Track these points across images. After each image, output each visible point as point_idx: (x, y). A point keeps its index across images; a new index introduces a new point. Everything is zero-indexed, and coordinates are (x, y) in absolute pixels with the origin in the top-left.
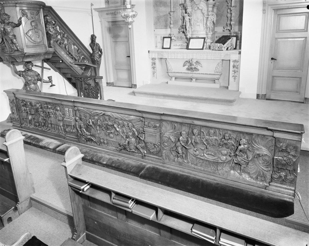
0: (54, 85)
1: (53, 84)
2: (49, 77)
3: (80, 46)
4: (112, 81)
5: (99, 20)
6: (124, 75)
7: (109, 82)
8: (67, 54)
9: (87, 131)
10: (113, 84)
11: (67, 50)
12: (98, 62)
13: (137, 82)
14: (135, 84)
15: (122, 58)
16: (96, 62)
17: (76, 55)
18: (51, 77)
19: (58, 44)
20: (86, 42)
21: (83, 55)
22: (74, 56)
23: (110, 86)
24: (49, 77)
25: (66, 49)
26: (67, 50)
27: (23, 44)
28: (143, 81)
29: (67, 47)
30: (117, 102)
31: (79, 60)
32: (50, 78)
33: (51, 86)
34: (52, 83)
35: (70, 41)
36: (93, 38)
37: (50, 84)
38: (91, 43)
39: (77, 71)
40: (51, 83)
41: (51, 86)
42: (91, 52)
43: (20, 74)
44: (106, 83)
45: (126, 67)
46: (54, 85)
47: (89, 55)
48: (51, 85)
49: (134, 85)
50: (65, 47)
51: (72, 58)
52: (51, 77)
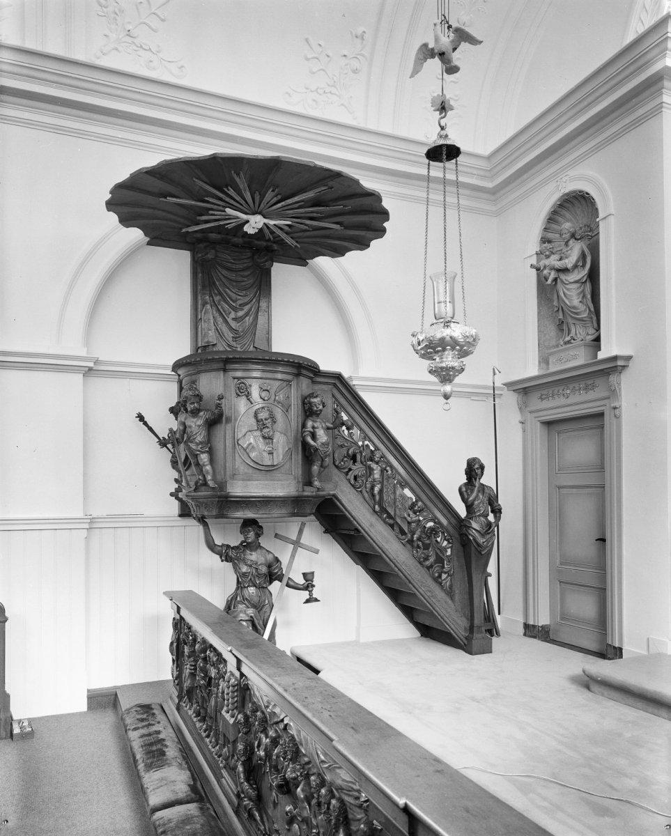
0: (316, 600)
1: (314, 596)
2: (304, 575)
3: (424, 491)
4: (543, 619)
5: (517, 417)
6: (584, 606)
7: (531, 622)
8: (374, 511)
9: (247, 780)
10: (548, 632)
11: (377, 498)
12: (479, 549)
13: (625, 639)
14: (617, 646)
15: (583, 548)
16: (473, 548)
17: (405, 518)
18: (313, 573)
19: (349, 481)
20: (449, 482)
21: (434, 519)
22: (399, 521)
23: (535, 637)
24: (304, 575)
25: (373, 495)
26: (377, 498)
27: (228, 470)
28: (648, 639)
29: (377, 489)
30: (333, 695)
31: (414, 534)
32: (308, 577)
33: (308, 601)
34: (311, 595)
35: (390, 472)
36: (473, 470)
37: (305, 595)
38: (465, 484)
39: (402, 569)
40: (308, 592)
41: (308, 601)
42: (463, 512)
43: (226, 554)
44: (522, 626)
45: (589, 577)
46: (316, 600)
47: (453, 520)
48: (308, 597)
49: (614, 648)
50: (372, 488)
51: (392, 526)
52: (313, 573)
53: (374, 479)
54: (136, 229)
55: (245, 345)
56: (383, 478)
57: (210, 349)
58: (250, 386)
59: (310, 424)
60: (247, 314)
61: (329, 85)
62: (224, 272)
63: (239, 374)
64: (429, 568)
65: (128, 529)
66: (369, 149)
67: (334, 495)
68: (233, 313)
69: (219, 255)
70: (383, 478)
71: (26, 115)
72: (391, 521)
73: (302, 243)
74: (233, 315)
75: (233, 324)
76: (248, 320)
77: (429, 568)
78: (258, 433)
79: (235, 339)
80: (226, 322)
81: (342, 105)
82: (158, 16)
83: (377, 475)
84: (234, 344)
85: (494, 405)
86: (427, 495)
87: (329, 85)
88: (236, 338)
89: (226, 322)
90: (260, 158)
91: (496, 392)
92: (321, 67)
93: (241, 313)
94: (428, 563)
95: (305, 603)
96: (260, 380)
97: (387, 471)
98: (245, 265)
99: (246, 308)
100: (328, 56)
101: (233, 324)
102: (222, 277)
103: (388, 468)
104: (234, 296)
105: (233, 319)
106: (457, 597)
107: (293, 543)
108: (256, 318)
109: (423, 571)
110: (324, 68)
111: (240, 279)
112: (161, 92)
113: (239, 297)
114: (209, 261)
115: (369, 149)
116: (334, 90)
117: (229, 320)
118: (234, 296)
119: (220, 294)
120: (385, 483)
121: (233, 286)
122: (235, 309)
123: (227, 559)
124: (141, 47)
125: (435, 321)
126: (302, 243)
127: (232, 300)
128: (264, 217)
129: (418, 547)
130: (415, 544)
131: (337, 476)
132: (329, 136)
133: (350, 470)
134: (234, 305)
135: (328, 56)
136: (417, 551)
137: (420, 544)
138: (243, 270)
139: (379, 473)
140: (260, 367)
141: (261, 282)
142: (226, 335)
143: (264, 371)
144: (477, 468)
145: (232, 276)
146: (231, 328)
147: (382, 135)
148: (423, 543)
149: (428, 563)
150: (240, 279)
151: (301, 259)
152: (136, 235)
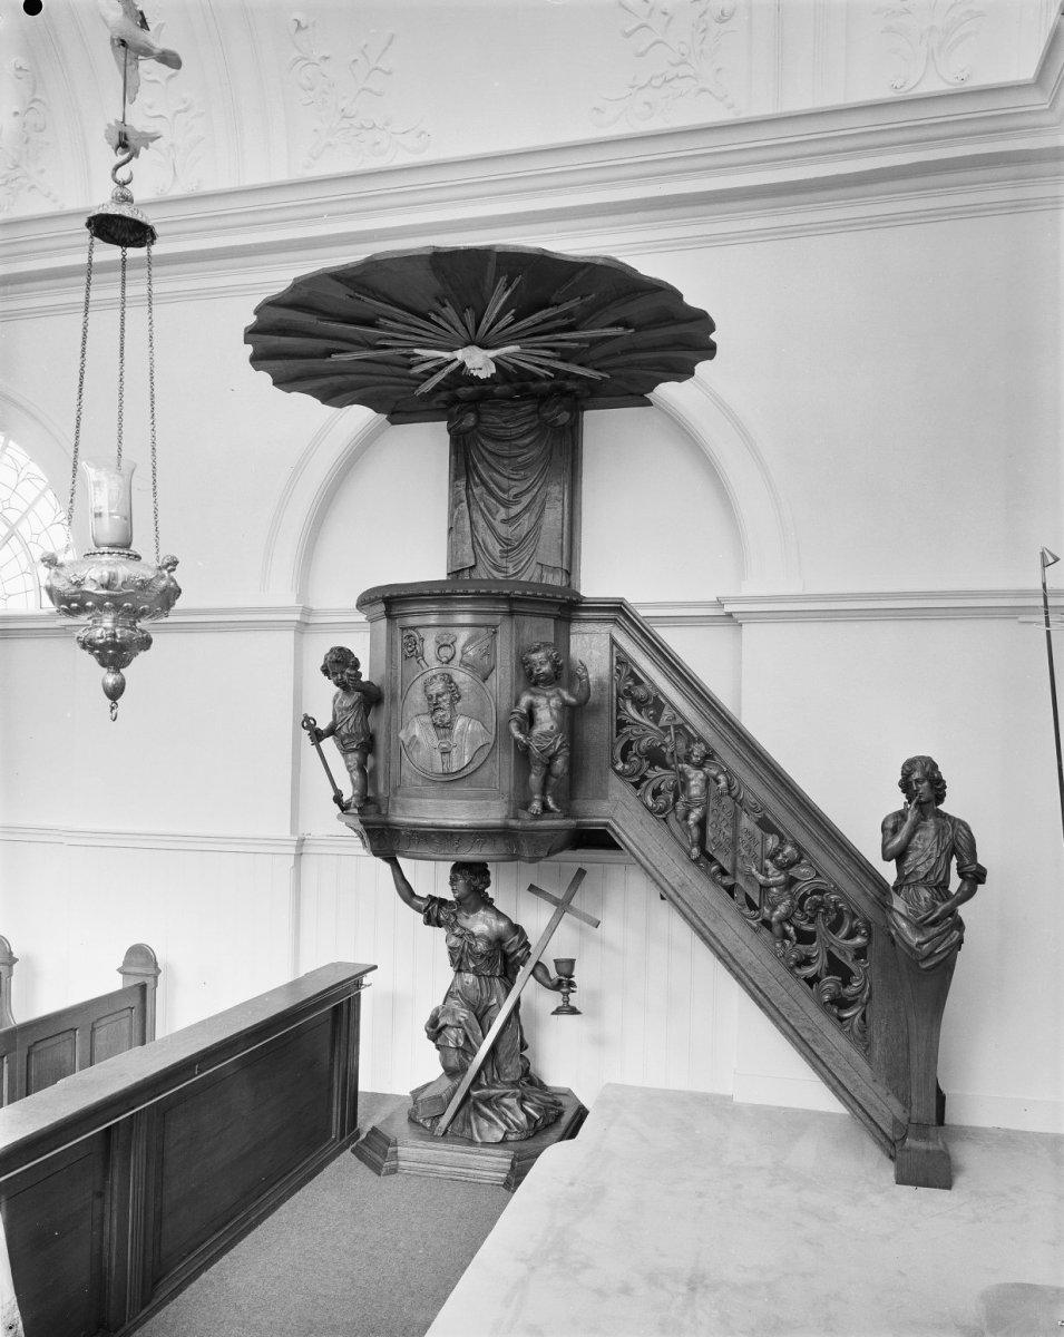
0: (574, 1011)
22: (741, 881)
32: (567, 967)
36: (923, 783)
43: (434, 912)
48: (561, 1004)
53: (690, 798)
54: (356, 407)
55: (521, 561)
56: (708, 797)
57: (466, 576)
58: (423, 640)
59: (526, 699)
60: (526, 509)
61: (673, 65)
62: (491, 446)
63: (412, 621)
64: (811, 981)
65: (355, 858)
66: (745, 158)
67: (607, 825)
68: (502, 510)
69: (484, 420)
70: (708, 797)
71: (194, 285)
72: (727, 881)
73: (614, 367)
74: (502, 513)
75: (502, 530)
76: (526, 522)
77: (811, 981)
78: (427, 719)
79: (505, 553)
80: (491, 528)
81: (703, 90)
82: (380, 70)
83: (695, 788)
84: (503, 562)
85: (1048, 632)
86: (810, 833)
87: (673, 65)
88: (507, 552)
89: (491, 528)
90: (351, 266)
91: (1050, 603)
92: (360, 87)
93: (515, 510)
94: (809, 971)
95: (579, 1013)
96: (438, 629)
97: (718, 782)
98: (526, 427)
99: (526, 500)
100: (665, 14)
101: (502, 530)
102: (486, 454)
103: (721, 777)
104: (505, 483)
105: (503, 521)
106: (877, 1052)
107: (556, 902)
108: (540, 517)
109: (798, 989)
110: (660, 38)
111: (517, 451)
112: (432, 181)
113: (513, 483)
114: (468, 432)
115: (745, 158)
116: (682, 70)
117: (496, 524)
118: (505, 483)
119: (484, 483)
120: (713, 804)
121: (504, 466)
122: (506, 504)
123: (432, 920)
124: (363, 127)
125: (94, 549)
126: (614, 367)
127: (499, 487)
128: (487, 348)
129: (785, 935)
130: (777, 929)
131: (619, 790)
132: (817, 140)
133: (644, 778)
134: (505, 496)
135: (665, 14)
136: (784, 945)
137: (791, 930)
138: (523, 436)
139: (702, 785)
140: (434, 607)
141: (551, 450)
142: (490, 548)
143: (441, 613)
144: (917, 781)
145: (503, 449)
146: (499, 538)
147: (716, 128)
148: (797, 930)
149: (809, 971)
150: (517, 451)
151: (634, 393)
152: (360, 416)
